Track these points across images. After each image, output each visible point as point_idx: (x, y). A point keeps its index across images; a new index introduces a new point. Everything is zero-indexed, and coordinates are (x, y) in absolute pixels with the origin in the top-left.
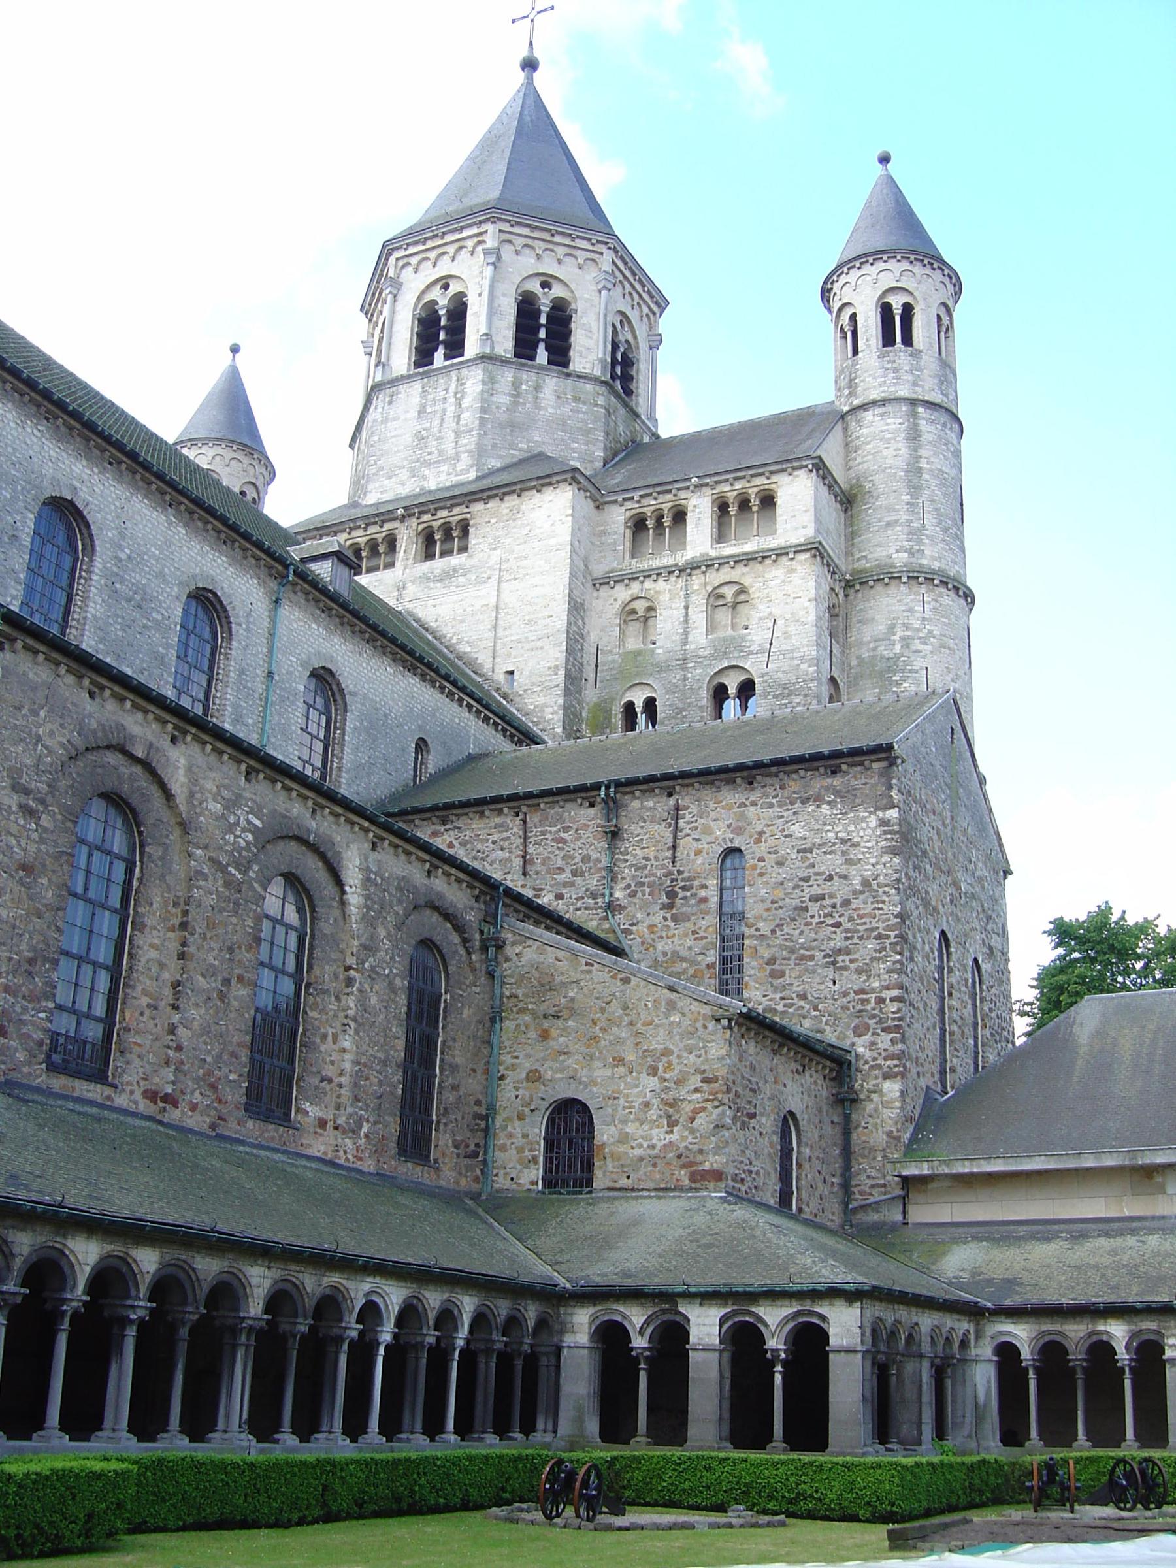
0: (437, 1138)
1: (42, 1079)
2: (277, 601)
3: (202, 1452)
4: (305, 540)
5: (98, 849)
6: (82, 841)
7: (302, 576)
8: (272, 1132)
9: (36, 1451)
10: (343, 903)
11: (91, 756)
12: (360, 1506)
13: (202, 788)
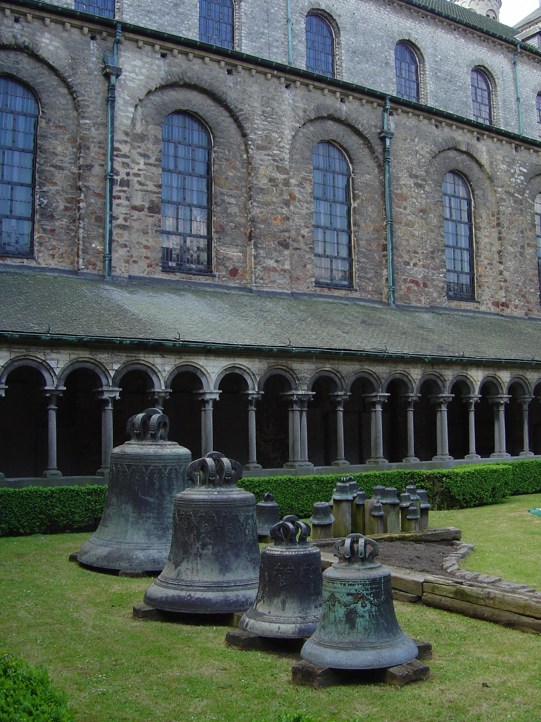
1: (446, 303)
2: (514, 63)
4: (522, 31)
5: (453, 196)
6: (445, 194)
7: (524, 48)
9: (467, 463)
11: (442, 155)
13: (496, 160)
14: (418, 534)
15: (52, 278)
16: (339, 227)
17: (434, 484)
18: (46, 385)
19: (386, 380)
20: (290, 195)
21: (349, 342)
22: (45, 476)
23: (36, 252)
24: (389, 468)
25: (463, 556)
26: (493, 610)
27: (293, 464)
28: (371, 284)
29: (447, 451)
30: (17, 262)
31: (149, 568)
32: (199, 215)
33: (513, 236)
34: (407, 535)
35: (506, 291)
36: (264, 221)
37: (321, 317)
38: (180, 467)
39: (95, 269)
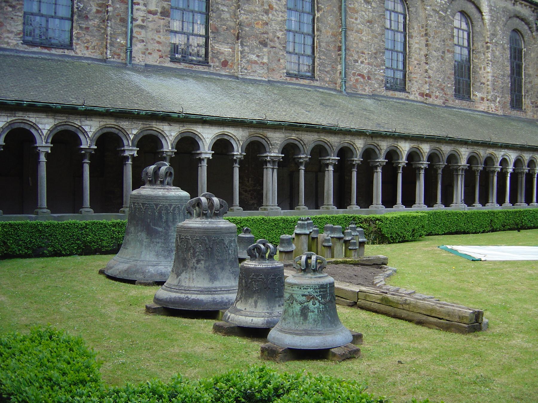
0: (525, 101)
1: (384, 93)
3: (448, 210)
5: (393, 11)
6: (387, 10)
8: (465, 103)
9: (395, 211)
10: (483, 19)
12: (504, 227)
14: (357, 260)
15: (87, 64)
16: (305, 31)
17: (370, 225)
18: (81, 145)
19: (337, 147)
20: (269, 6)
21: (310, 118)
22: (81, 213)
23: (74, 44)
24: (337, 213)
25: (389, 276)
26: (408, 312)
27: (265, 208)
28: (329, 76)
29: (380, 202)
30: (60, 52)
31: (158, 279)
32: (199, 19)
33: (436, 44)
34: (348, 260)
35: (430, 85)
36: (249, 25)
37: (290, 99)
38: (182, 205)
39: (119, 58)
